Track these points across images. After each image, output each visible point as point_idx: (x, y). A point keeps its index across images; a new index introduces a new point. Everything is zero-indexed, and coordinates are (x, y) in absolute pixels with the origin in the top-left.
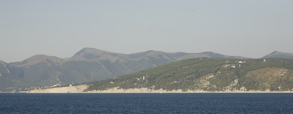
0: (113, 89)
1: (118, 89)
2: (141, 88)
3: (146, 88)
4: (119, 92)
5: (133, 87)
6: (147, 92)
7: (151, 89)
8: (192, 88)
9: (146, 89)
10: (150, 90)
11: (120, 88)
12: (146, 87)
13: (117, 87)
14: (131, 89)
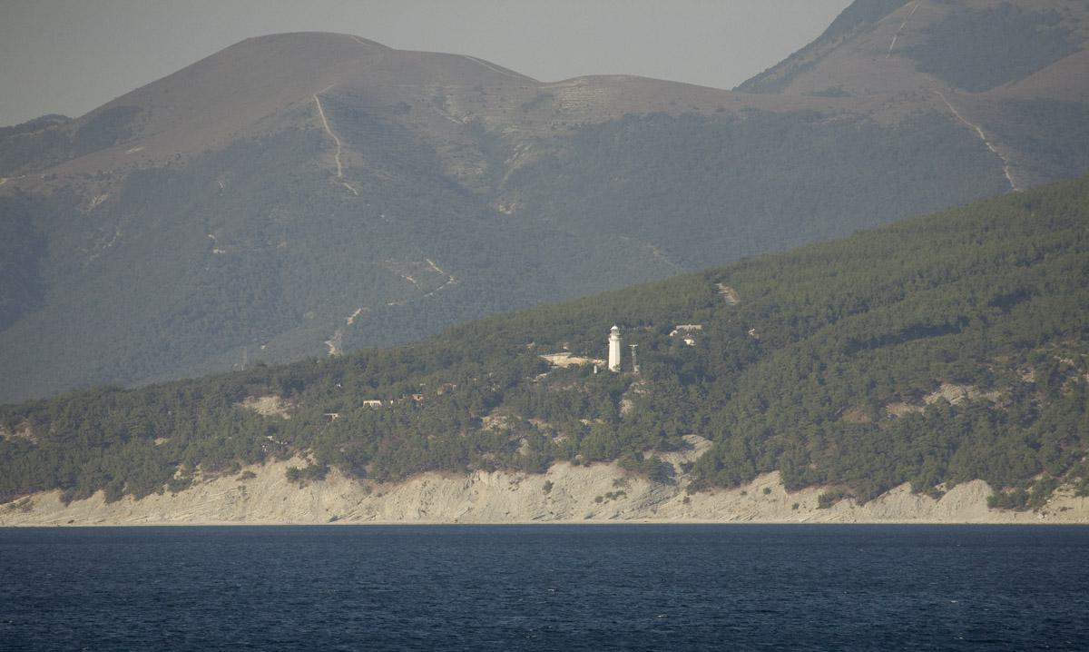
0: (249, 484)
1: (294, 475)
3: (600, 468)
5: (458, 460)
6: (604, 516)
7: (661, 475)
9: (603, 476)
10: (640, 486)
11: (318, 473)
12: (603, 460)
13: (299, 463)
14: (433, 479)
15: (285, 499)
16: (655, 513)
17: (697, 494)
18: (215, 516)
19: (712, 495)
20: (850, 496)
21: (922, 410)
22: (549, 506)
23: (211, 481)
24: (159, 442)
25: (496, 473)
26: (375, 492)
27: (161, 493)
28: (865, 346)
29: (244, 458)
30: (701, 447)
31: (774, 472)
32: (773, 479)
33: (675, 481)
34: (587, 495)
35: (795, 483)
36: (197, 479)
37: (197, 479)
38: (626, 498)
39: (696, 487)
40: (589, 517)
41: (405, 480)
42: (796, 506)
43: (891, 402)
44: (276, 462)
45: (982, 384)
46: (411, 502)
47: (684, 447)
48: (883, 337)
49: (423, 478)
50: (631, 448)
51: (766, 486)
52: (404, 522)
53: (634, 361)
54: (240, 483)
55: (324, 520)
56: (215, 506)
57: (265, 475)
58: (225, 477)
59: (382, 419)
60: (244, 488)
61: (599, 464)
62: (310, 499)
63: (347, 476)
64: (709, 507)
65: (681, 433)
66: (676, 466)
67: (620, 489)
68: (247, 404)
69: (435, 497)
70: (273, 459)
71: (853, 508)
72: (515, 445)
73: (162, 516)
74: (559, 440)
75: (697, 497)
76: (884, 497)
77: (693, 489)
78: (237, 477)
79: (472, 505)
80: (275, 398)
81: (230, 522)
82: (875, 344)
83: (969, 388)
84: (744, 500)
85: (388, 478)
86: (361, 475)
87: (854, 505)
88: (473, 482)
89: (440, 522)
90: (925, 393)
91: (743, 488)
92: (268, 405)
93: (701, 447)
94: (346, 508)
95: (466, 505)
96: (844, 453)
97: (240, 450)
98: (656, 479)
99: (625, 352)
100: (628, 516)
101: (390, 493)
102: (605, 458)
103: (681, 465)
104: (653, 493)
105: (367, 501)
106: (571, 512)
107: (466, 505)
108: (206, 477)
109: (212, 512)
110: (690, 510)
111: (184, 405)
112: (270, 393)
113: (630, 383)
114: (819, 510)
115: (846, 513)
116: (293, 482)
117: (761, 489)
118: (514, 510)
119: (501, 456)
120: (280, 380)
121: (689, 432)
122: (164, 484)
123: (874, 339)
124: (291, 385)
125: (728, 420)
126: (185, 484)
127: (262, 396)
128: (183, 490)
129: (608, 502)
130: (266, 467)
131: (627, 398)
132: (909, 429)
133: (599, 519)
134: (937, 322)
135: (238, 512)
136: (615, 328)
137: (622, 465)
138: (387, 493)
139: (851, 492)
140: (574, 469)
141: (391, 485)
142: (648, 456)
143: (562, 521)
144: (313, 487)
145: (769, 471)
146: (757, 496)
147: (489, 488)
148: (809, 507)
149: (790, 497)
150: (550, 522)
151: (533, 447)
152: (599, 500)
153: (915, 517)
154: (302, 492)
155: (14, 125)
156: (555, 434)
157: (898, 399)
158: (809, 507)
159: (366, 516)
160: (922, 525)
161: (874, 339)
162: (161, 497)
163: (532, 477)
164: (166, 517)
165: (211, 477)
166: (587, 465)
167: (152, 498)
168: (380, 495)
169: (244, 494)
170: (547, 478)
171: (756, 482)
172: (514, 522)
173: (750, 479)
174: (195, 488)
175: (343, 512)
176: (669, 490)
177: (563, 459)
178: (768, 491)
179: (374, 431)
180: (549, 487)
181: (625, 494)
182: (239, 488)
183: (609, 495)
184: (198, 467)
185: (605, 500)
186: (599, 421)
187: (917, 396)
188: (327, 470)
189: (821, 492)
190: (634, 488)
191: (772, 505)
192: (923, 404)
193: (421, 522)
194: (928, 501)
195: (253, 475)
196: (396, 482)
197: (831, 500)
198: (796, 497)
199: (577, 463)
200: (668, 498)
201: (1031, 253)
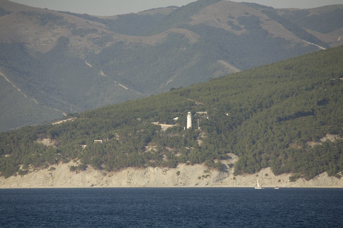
0: (53, 172)
1: (73, 169)
3: (197, 166)
5: (141, 162)
6: (203, 184)
7: (222, 169)
9: (200, 169)
10: (215, 173)
11: (83, 168)
12: (199, 163)
13: (72, 163)
14: (131, 170)
15: (70, 178)
16: (222, 183)
17: (238, 176)
18: (40, 185)
19: (244, 176)
20: (302, 177)
21: (321, 144)
22: (180, 180)
23: (37, 171)
24: (6, 156)
25: (156, 168)
26: (108, 175)
27: (16, 176)
28: (283, 120)
29: (50, 162)
30: (235, 159)
31: (268, 168)
32: (268, 170)
33: (227, 171)
34: (193, 177)
35: (278, 172)
36: (30, 170)
37: (30, 170)
38: (210, 177)
39: (236, 173)
40: (197, 185)
41: (119, 170)
42: (279, 181)
43: (308, 141)
44: (63, 164)
45: (341, 134)
47: (227, 158)
48: (289, 116)
49: (127, 170)
50: (209, 158)
51: (265, 173)
52: (122, 186)
53: (198, 125)
54: (50, 172)
55: (88, 186)
56: (40, 181)
57: (59, 169)
59: (105, 147)
60: (51, 173)
61: (197, 164)
62: (81, 178)
63: (96, 169)
64: (244, 181)
65: (226, 152)
66: (226, 165)
67: (207, 174)
68: (38, 142)
69: (133, 177)
70: (61, 162)
71: (304, 182)
72: (161, 157)
73: (18, 184)
74: (178, 155)
75: (238, 177)
76: (317, 177)
77: (236, 174)
78: (48, 169)
79: (149, 180)
81: (47, 186)
82: (286, 119)
83: (336, 136)
84: (258, 178)
85: (113, 170)
86: (101, 168)
87: (304, 180)
88: (147, 171)
90: (320, 138)
91: (256, 174)
92: (46, 142)
93: (235, 159)
94: (97, 181)
95: (147, 180)
96: (296, 161)
97: (45, 160)
98: (220, 170)
99: (193, 122)
100: (212, 184)
101: (114, 176)
102: (199, 162)
103: (229, 165)
104: (220, 176)
105: (105, 178)
107: (147, 180)
108: (34, 170)
109: (39, 183)
110: (236, 182)
111: (14, 142)
112: (46, 138)
113: (199, 133)
114: (291, 183)
115: (301, 184)
116: (72, 171)
117: (264, 174)
118: (166, 182)
119: (156, 161)
120: (50, 132)
121: (229, 152)
122: (16, 172)
123: (286, 117)
124: (54, 135)
125: (241, 148)
126: (26, 172)
127: (43, 138)
128: (26, 174)
129: (203, 179)
130: (59, 166)
131: (199, 139)
132: (318, 151)
133: (201, 185)
134: (306, 111)
135: (50, 183)
136: (189, 112)
137: (206, 165)
138: (113, 175)
139: (302, 175)
140: (187, 166)
141: (114, 172)
142: (216, 161)
144: (82, 173)
145: (266, 167)
146: (263, 177)
147: (154, 174)
148: (285, 181)
149: (276, 177)
150: (181, 187)
151: (169, 158)
152: (199, 178)
153: (331, 185)
154: (78, 175)
155: (264, 5)
156: (176, 153)
157: (311, 140)
158: (285, 181)
159: (106, 184)
160: (330, 188)
161: (286, 117)
162: (16, 177)
163: (171, 169)
164: (20, 185)
165: (37, 169)
166: (192, 165)
167: (12, 177)
168: (110, 176)
169: (52, 176)
170: (177, 170)
171: (261, 171)
173: (259, 171)
174: (31, 174)
175: (96, 183)
176: (226, 174)
177: (182, 162)
178: (267, 175)
179: (103, 152)
180: (178, 173)
181: (210, 176)
182: (49, 173)
183: (203, 176)
184: (30, 165)
185: (202, 178)
186: (192, 148)
187: (318, 139)
188: (87, 167)
189: (290, 175)
191: (269, 180)
192: (320, 142)
193: (129, 186)
194: (336, 179)
195: (54, 169)
196: (116, 171)
197: (295, 178)
198: (279, 177)
199: (188, 164)
201: (310, 86)
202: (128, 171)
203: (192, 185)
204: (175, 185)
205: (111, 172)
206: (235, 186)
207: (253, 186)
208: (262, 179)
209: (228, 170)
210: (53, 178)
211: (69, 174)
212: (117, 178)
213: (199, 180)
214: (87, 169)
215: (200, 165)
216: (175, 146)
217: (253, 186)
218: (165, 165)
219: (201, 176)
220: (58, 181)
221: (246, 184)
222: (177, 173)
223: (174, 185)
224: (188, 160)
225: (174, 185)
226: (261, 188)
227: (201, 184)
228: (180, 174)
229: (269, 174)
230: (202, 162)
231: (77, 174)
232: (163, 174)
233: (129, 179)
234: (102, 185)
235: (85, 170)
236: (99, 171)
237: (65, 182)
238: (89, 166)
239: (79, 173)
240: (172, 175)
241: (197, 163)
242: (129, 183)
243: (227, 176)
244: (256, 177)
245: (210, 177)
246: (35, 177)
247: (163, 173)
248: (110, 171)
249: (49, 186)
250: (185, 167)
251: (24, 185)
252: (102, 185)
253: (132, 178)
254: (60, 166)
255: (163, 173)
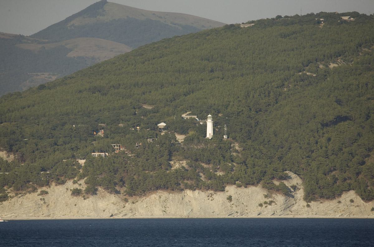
0: (46, 197)
1: (76, 193)
2: (223, 190)
3: (252, 189)
4: (93, 216)
5: (174, 183)
6: (268, 213)
7: (288, 193)
8: (204, 118)
9: (256, 193)
10: (280, 198)
11: (92, 191)
12: (253, 184)
13: (70, 184)
14: (164, 194)
15: (75, 205)
16: (292, 212)
17: (312, 202)
18: (31, 215)
19: (321, 203)
23: (22, 196)
25: (197, 191)
32: (352, 194)
34: (248, 203)
38: (276, 204)
40: (259, 214)
46: (155, 206)
49: (158, 194)
51: (350, 199)
53: (225, 132)
54: (40, 197)
55: (106, 216)
58: (246, 187)
60: (44, 199)
61: (252, 186)
63: (111, 193)
67: (270, 199)
70: (54, 184)
78: (37, 193)
80: (5, 152)
89: (174, 217)
101: (139, 202)
102: (254, 183)
106: (247, 212)
108: (17, 194)
130: (51, 188)
136: (210, 116)
138: (137, 201)
140: (239, 189)
143: (244, 217)
144: (92, 199)
145: (349, 190)
149: (367, 204)
163: (219, 193)
165: (20, 194)
168: (133, 203)
169: (45, 203)
172: (216, 217)
173: (340, 195)
174: (13, 200)
175: (116, 212)
181: (275, 202)
182: (41, 199)
185: (264, 206)
188: (96, 190)
190: (277, 199)
196: (140, 196)
199: (239, 186)
200: (293, 204)
202: (160, 196)
203: (253, 214)
204: (280, 215)
205: (134, 197)
206: (311, 216)
207: (122, 215)
208: (347, 206)
209: (293, 194)
210: (47, 206)
211: (72, 199)
212: (145, 206)
213: (260, 207)
214: (97, 192)
215: (256, 187)
216: (212, 162)
217: (122, 215)
218: (208, 188)
219: (262, 203)
220: (55, 209)
221: (326, 214)
222: (228, 199)
223: (229, 215)
224: (237, 181)
225: (229, 215)
226: (3, 221)
227: (265, 213)
228: (232, 200)
229: (355, 200)
230: (258, 183)
231: (85, 199)
232: (209, 199)
233: (164, 207)
234: (125, 215)
235: (96, 194)
236: (116, 195)
237: (69, 211)
238: (100, 189)
239: (88, 199)
240: (222, 200)
241: (252, 185)
242: (164, 212)
243: (294, 202)
244: (338, 204)
245: (276, 204)
246: (21, 204)
247: (208, 198)
248: (132, 196)
249: (45, 217)
250: (236, 189)
251: (5, 216)
252: (125, 215)
253: (168, 206)
254: (53, 188)
255: (208, 198)
